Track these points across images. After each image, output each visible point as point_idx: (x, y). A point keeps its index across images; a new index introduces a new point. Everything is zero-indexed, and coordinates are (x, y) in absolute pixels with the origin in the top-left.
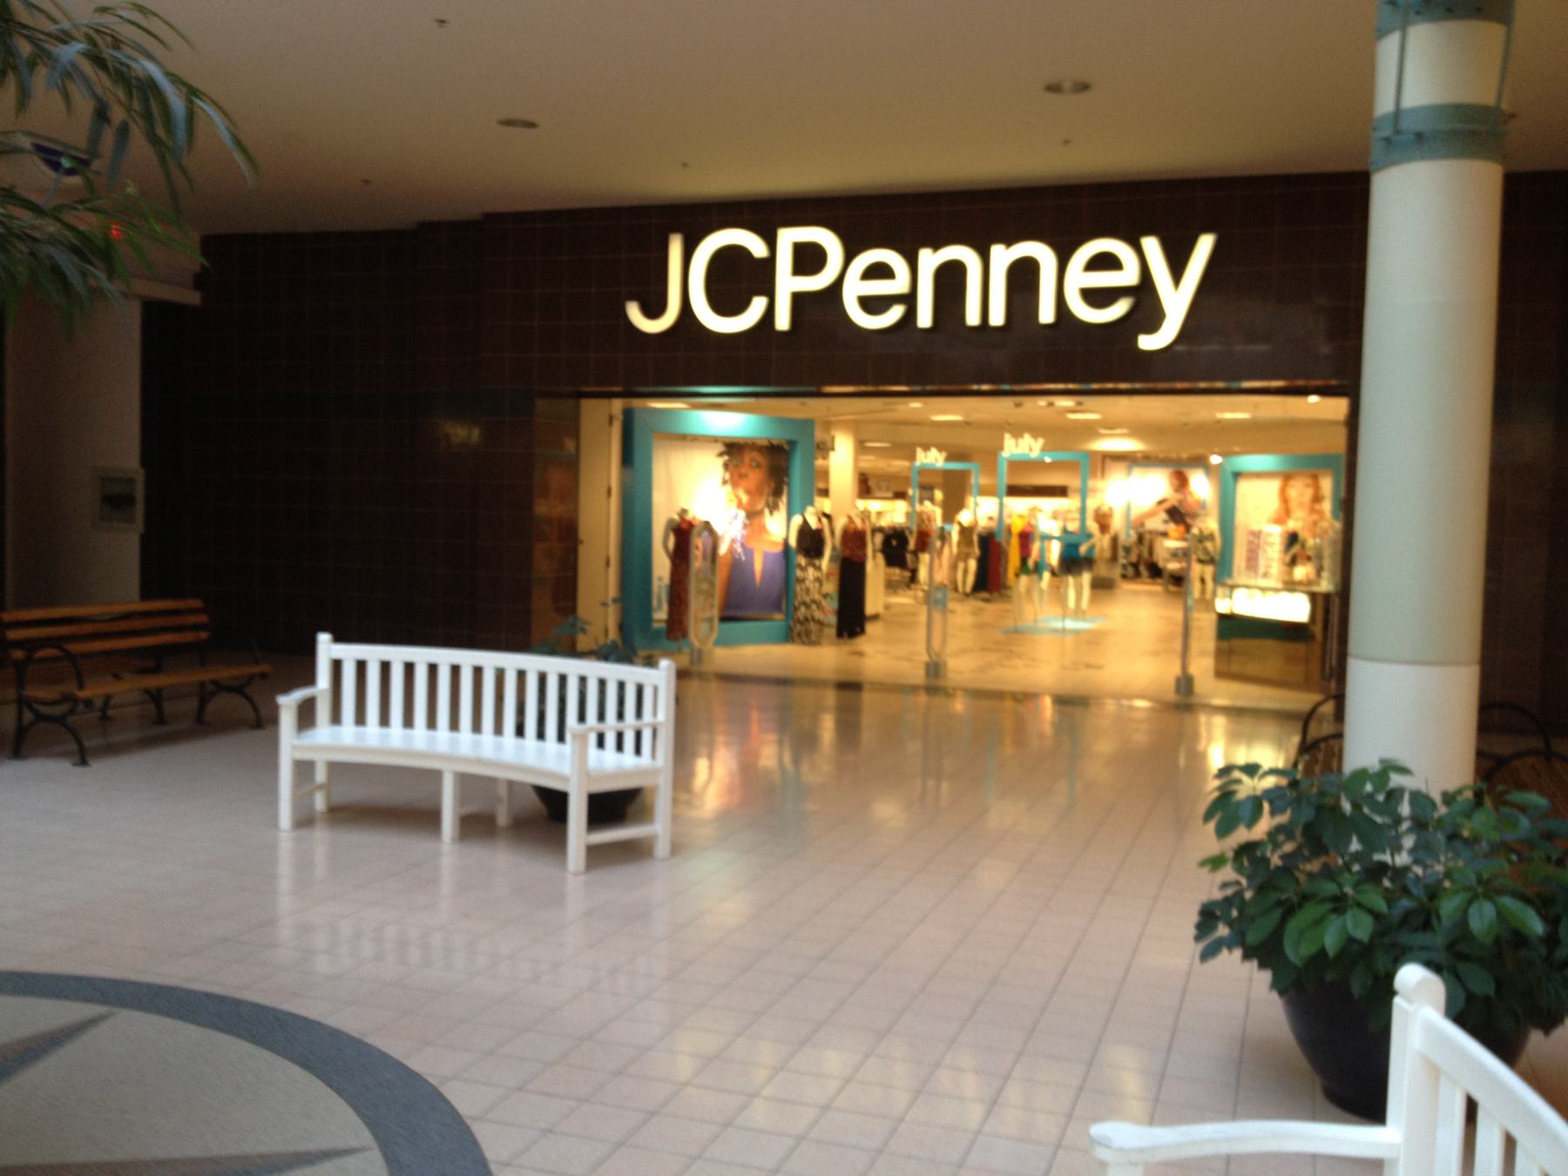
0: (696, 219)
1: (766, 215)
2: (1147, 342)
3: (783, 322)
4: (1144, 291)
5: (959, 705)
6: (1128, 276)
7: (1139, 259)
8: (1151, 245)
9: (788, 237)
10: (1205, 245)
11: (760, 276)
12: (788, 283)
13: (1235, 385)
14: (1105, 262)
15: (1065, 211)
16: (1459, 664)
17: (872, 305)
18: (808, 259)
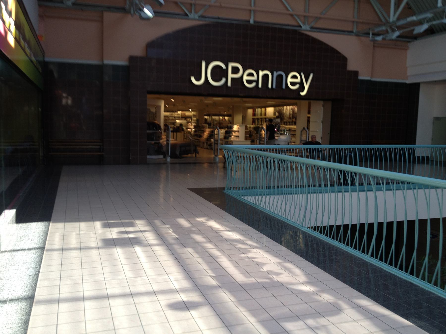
2: (303, 94)
3: (229, 84)
4: (301, 84)
6: (298, 80)
9: (231, 65)
11: (225, 73)
17: (249, 82)
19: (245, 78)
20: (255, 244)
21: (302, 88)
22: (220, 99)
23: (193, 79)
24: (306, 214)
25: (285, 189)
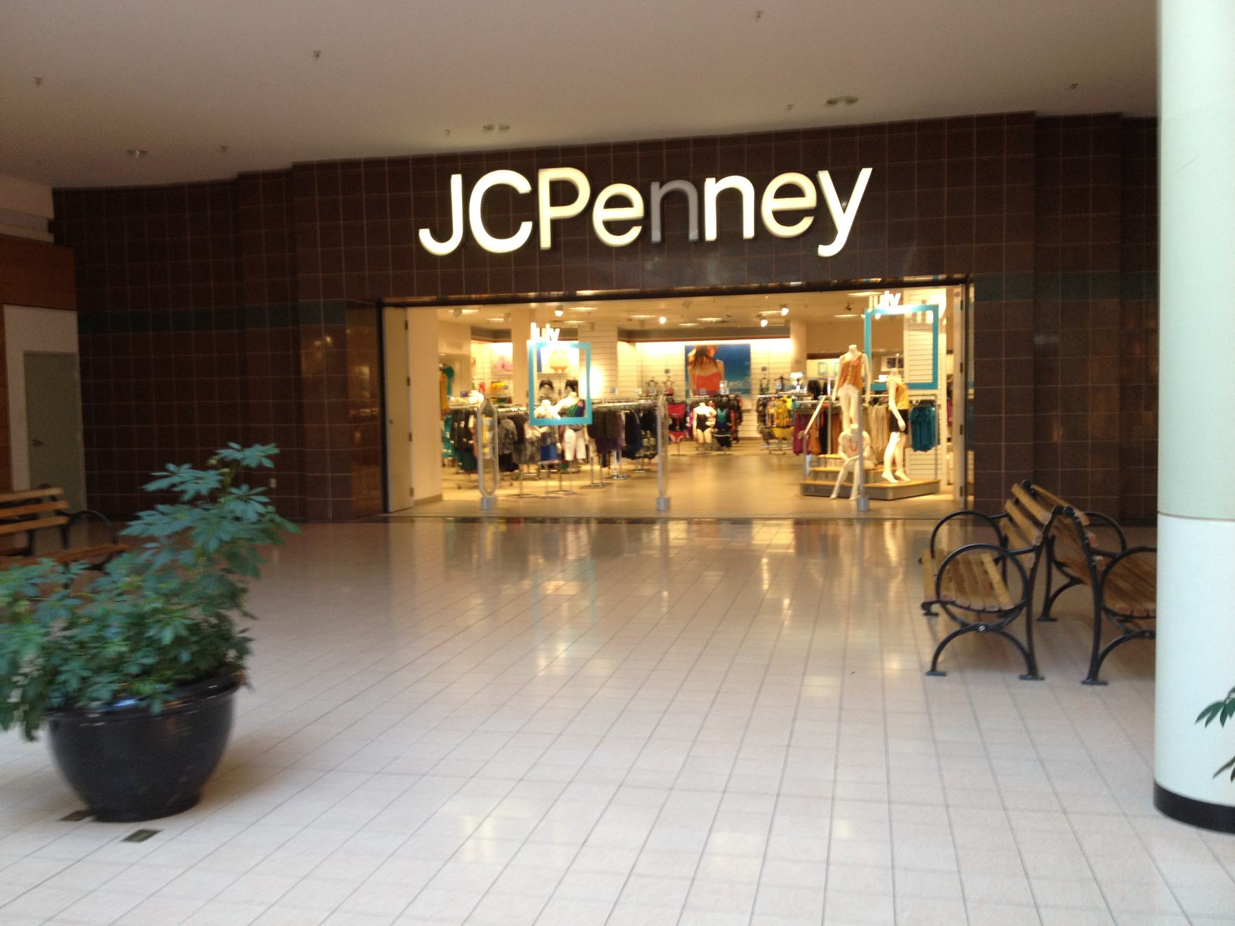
0: (473, 165)
1: (529, 160)
2: (825, 251)
3: (546, 242)
4: (821, 211)
5: (677, 532)
6: (809, 201)
7: (813, 188)
8: (825, 177)
9: (547, 176)
10: (865, 175)
11: (527, 207)
12: (548, 213)
13: (546, 294)
14: (791, 191)
15: (762, 154)
16: (387, 532)
17: (616, 227)
18: (563, 193)
19: (601, 214)
20: (854, 593)
21: (823, 226)
22: (793, 283)
23: (425, 235)
24: (1060, 596)
25: (646, 460)
